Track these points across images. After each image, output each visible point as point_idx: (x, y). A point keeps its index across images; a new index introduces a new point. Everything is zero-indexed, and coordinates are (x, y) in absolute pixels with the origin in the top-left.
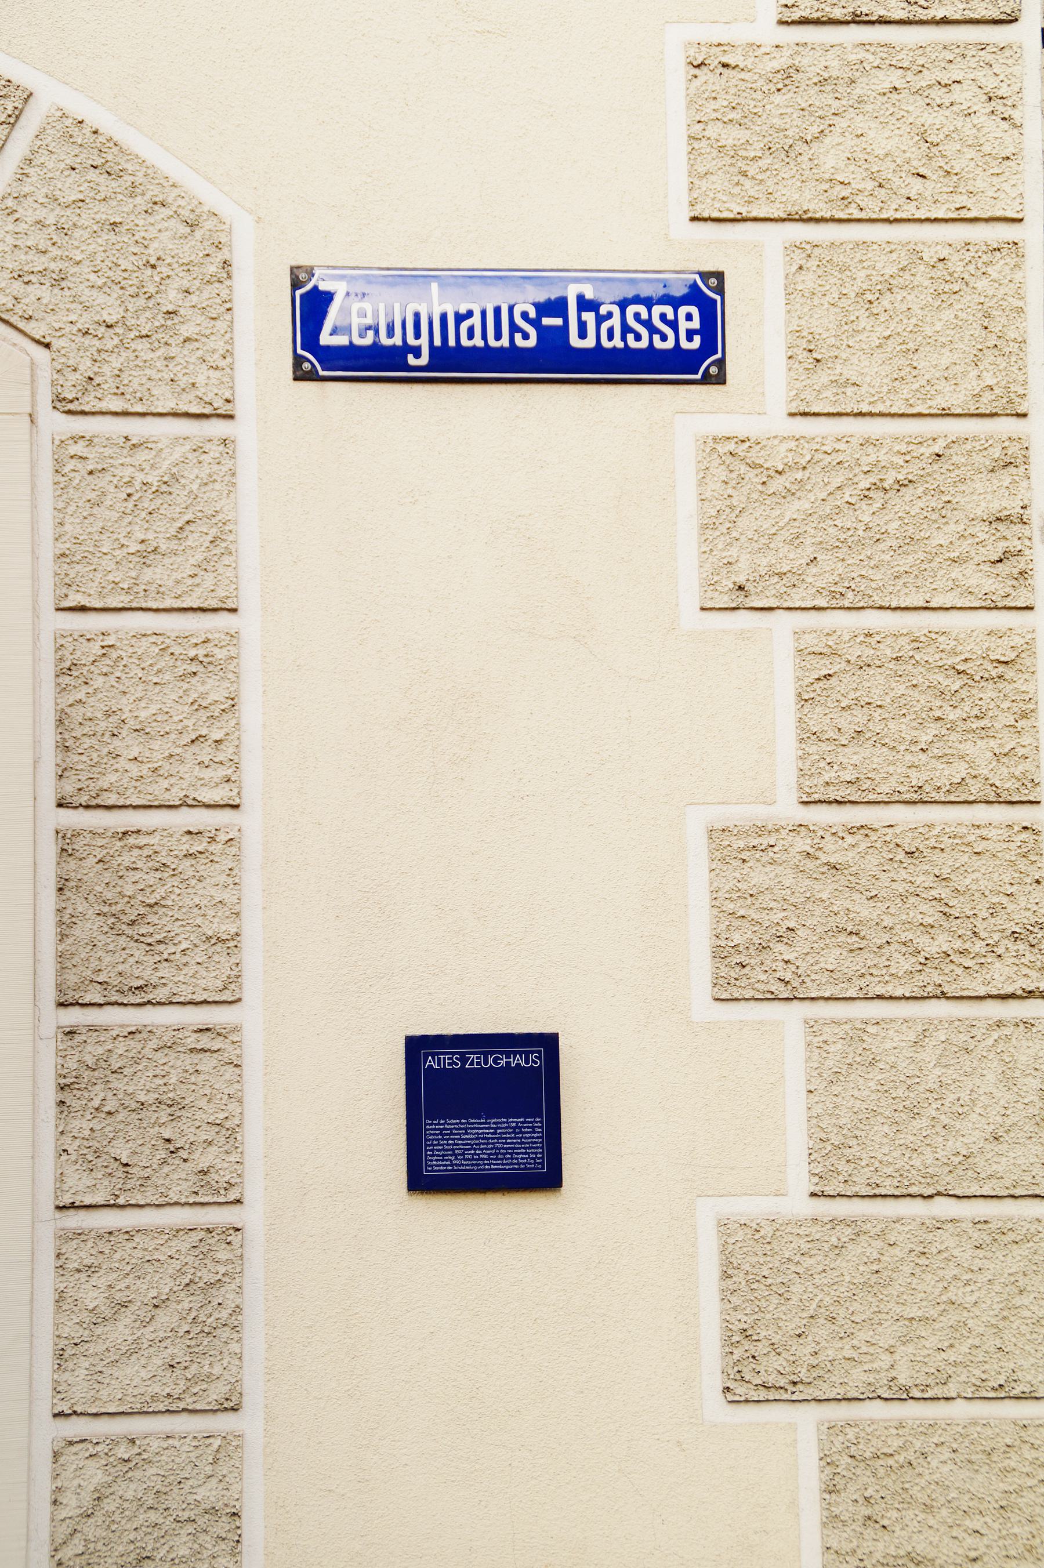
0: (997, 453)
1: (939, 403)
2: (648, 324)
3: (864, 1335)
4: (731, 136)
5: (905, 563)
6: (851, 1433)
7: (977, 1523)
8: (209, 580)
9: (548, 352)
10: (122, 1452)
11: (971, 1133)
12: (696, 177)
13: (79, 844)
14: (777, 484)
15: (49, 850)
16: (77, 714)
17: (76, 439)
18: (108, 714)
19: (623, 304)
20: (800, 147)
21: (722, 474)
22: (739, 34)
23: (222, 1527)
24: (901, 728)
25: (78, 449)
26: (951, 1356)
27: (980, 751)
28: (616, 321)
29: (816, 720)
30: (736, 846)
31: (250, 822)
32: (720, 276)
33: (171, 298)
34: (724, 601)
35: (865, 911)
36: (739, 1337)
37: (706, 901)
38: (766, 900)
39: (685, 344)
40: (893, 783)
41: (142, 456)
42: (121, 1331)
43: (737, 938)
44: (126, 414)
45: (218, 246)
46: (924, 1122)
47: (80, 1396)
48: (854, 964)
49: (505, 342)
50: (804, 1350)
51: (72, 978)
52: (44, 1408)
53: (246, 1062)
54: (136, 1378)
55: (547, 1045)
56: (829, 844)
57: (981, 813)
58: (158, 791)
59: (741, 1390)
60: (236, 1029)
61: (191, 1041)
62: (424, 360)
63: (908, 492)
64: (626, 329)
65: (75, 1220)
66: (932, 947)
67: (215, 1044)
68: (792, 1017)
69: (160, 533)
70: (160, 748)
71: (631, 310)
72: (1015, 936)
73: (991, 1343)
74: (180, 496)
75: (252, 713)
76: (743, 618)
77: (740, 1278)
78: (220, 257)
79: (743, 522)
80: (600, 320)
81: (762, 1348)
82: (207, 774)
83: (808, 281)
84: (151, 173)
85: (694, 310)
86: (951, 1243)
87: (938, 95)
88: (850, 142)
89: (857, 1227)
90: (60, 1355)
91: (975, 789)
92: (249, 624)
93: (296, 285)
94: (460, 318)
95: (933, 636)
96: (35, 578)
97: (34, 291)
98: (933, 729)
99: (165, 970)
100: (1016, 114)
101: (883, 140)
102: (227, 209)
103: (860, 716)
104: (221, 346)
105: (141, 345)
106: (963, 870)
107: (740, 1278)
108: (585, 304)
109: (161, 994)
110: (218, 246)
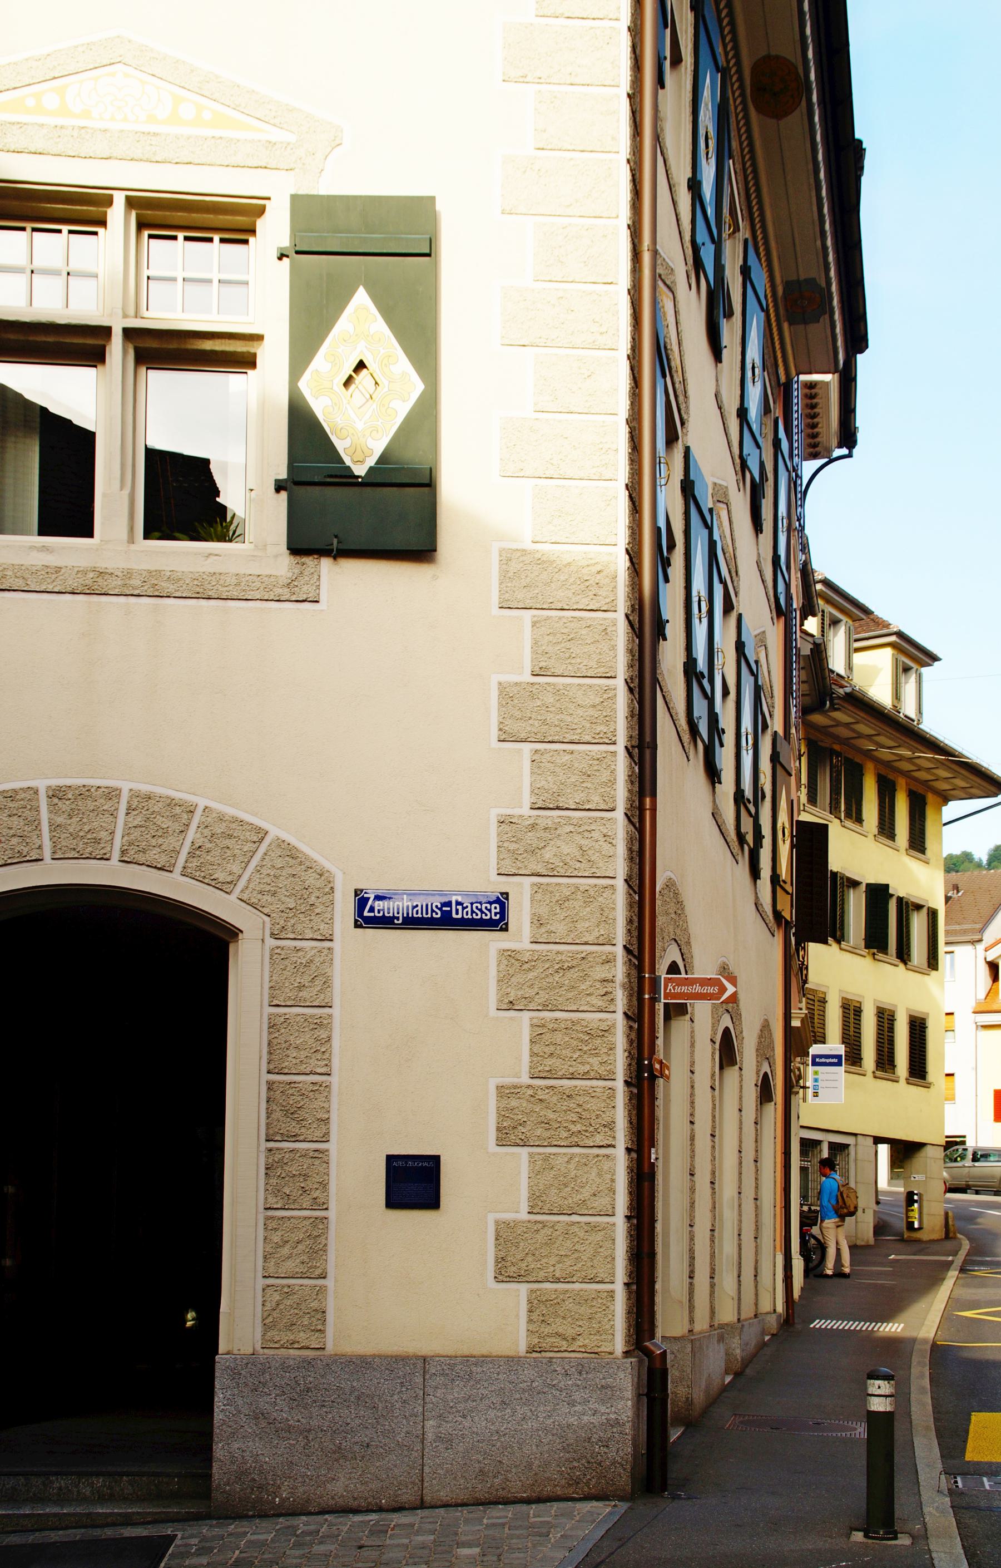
0: (604, 957)
1: (584, 939)
2: (481, 910)
3: (544, 1260)
4: (513, 846)
5: (570, 995)
6: (538, 1293)
7: (580, 1323)
8: (322, 996)
9: (445, 920)
10: (286, 1290)
11: (586, 1193)
12: (500, 860)
13: (275, 1085)
14: (526, 966)
15: (264, 1088)
16: (275, 1041)
17: (278, 947)
18: (286, 1042)
19: (472, 904)
20: (537, 851)
21: (506, 962)
22: (517, 812)
23: (319, 1316)
24: (567, 1052)
25: (278, 951)
26: (575, 1268)
27: (594, 1061)
28: (469, 909)
29: (536, 1049)
30: (507, 694)
31: (334, 1080)
32: (507, 894)
33: (312, 899)
34: (505, 1007)
35: (551, 1115)
36: (500, 1261)
37: (495, 1111)
38: (516, 1111)
39: (494, 917)
40: (563, 1071)
41: (300, 954)
42: (286, 1251)
43: (505, 1124)
44: (295, 939)
45: (329, 882)
46: (569, 1189)
47: (272, 1270)
48: (548, 1134)
49: (429, 915)
50: (523, 1265)
51: (271, 1132)
52: (260, 1275)
53: (330, 1162)
54: (290, 1266)
55: (436, 1159)
56: (540, 1092)
57: (595, 1083)
58: (302, 1068)
59: (501, 1278)
60: (327, 1151)
61: (311, 1154)
62: (400, 922)
63: (572, 971)
64: (473, 912)
65: (270, 1213)
66: (574, 1128)
67: (321, 1156)
68: (524, 1151)
69: (306, 980)
70: (303, 1054)
71: (474, 906)
72: (605, 1126)
73: (589, 1264)
74: (313, 967)
75: (336, 1042)
76: (512, 1013)
77: (502, 1240)
78: (330, 886)
79: (513, 979)
80: (464, 908)
81: (508, 1264)
82: (319, 1063)
83: (538, 896)
84: (307, 857)
85: (497, 906)
86: (577, 1230)
87: (586, 834)
88: (555, 849)
89: (544, 1224)
90: (265, 1257)
91: (592, 1074)
92: (336, 1011)
93: (356, 895)
94: (414, 907)
95: (578, 1022)
96: (262, 995)
97: (265, 897)
98: (578, 1053)
99: (303, 1130)
100: (614, 842)
101: (566, 849)
102: (333, 869)
103: (552, 1048)
104: (329, 916)
105: (301, 916)
106: (587, 1102)
107: (502, 1240)
108: (458, 903)
109: (301, 1138)
110: (329, 882)
